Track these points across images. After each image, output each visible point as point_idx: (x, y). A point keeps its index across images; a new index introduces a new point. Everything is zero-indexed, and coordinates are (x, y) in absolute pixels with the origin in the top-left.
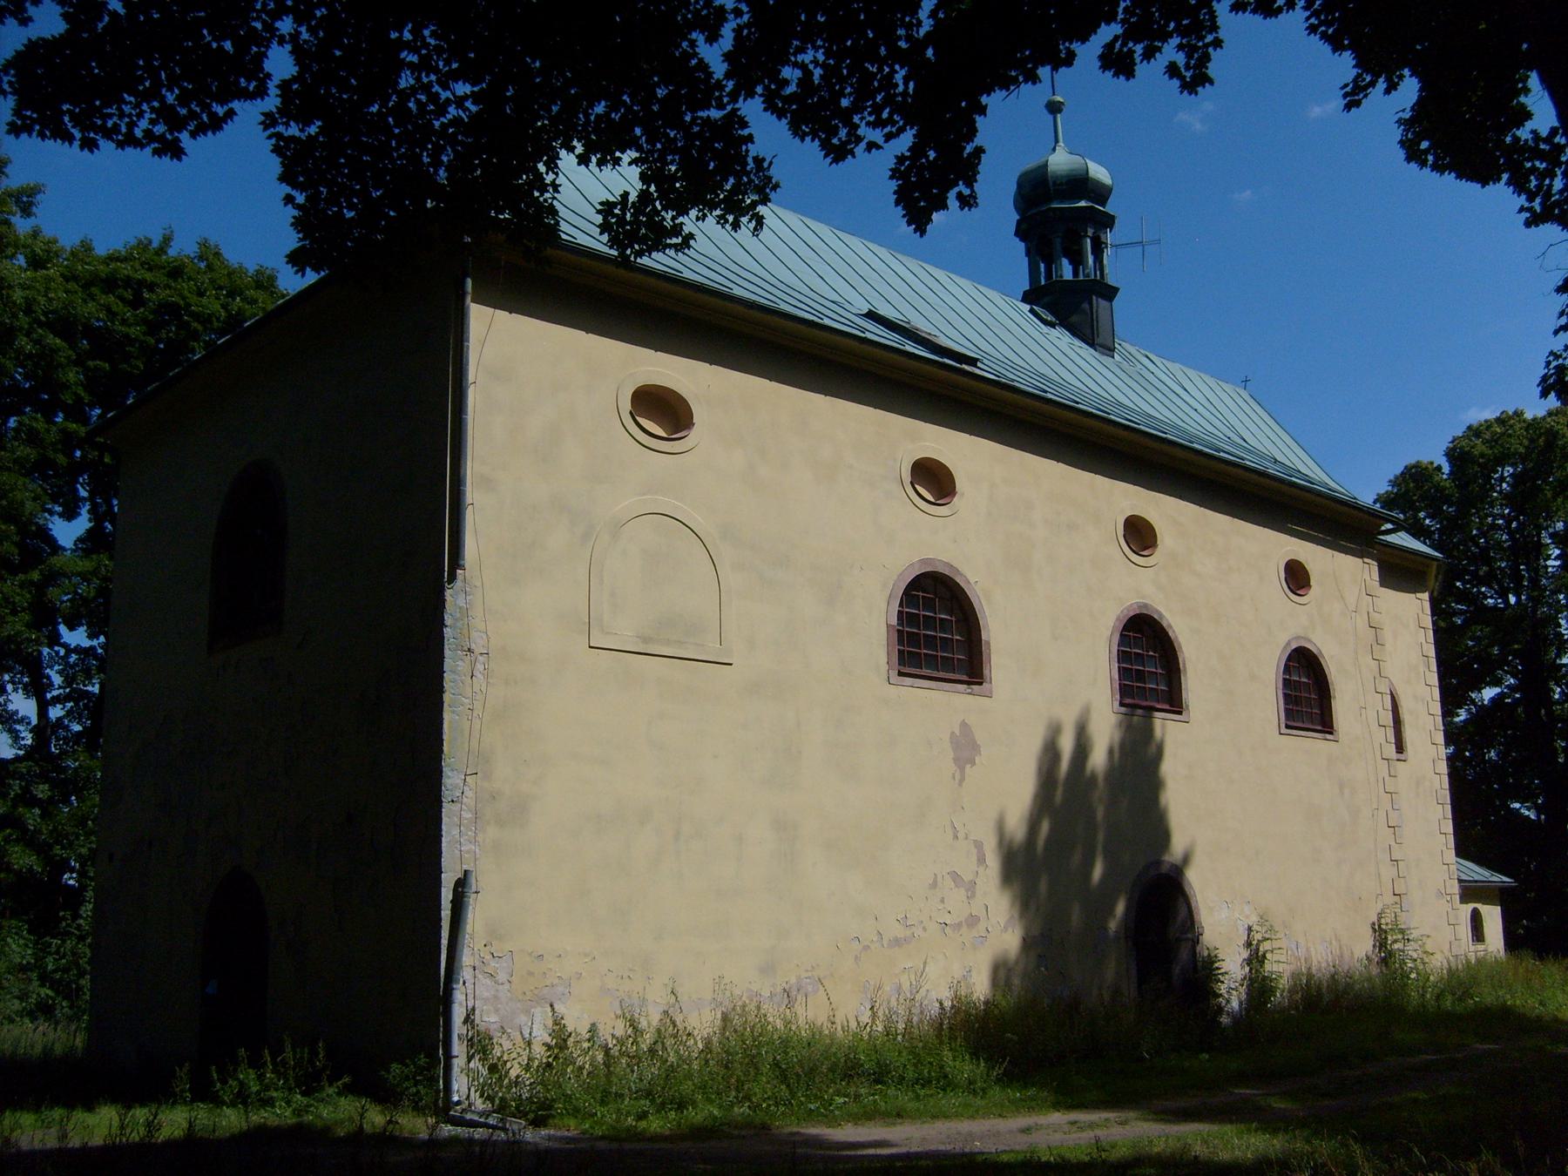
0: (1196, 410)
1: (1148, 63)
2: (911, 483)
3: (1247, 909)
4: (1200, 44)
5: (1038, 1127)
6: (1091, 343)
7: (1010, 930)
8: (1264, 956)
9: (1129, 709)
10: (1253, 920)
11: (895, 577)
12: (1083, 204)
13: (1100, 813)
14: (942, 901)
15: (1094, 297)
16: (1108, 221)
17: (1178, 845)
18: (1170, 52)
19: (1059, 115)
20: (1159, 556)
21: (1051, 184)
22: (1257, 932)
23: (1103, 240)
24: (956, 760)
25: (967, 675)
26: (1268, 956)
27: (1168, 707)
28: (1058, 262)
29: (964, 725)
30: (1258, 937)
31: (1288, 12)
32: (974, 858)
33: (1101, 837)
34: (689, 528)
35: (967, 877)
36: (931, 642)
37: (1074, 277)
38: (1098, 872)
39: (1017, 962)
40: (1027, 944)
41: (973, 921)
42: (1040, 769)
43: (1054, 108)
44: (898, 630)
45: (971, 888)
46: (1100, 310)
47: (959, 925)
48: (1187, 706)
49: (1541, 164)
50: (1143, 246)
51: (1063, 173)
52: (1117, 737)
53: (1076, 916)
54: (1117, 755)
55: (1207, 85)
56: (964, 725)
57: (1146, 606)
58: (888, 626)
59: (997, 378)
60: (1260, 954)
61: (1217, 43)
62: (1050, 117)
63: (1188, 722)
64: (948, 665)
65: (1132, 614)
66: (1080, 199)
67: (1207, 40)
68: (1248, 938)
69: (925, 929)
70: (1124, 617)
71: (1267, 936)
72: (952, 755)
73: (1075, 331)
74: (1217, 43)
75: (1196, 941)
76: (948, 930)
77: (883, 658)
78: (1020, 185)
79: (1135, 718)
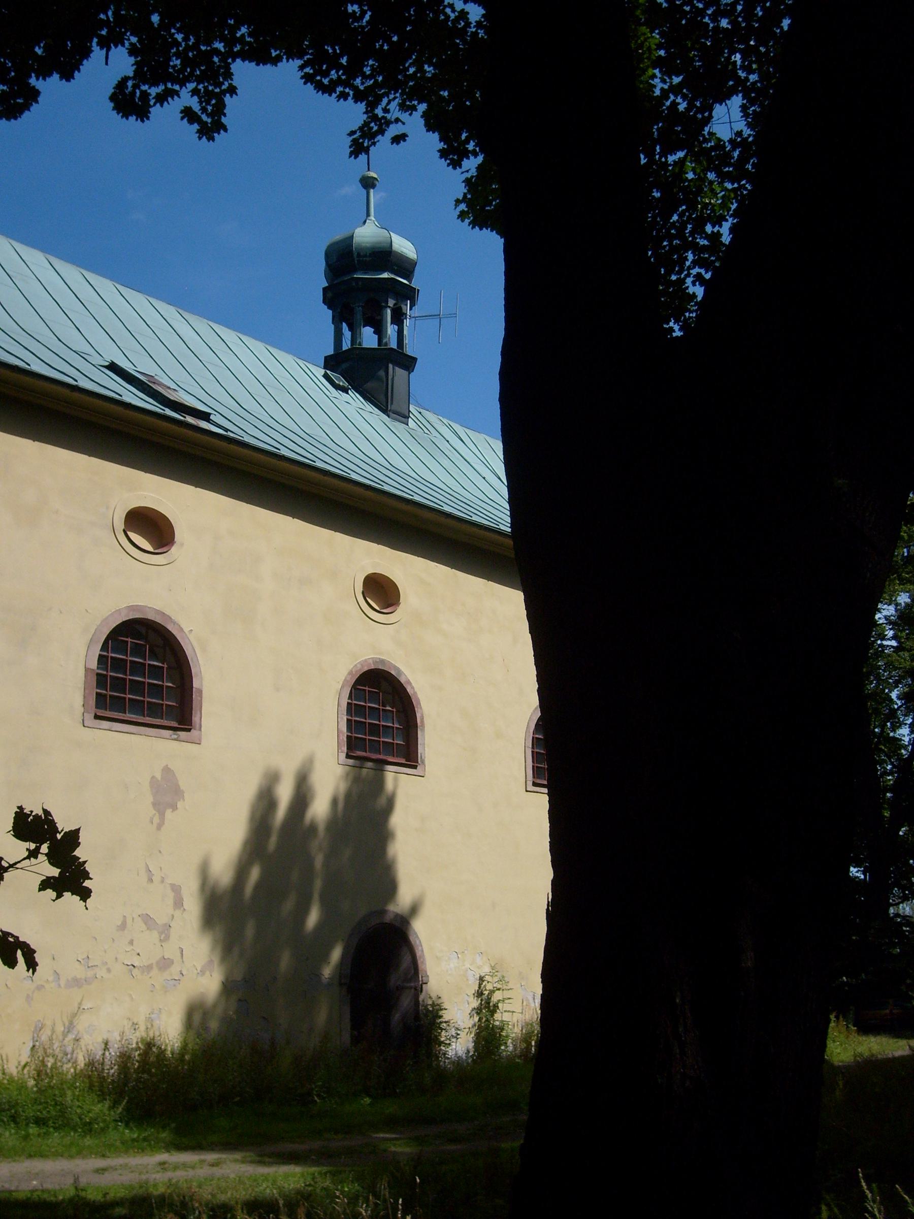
0: (484, 478)
1: (162, 106)
2: (124, 531)
3: (479, 961)
4: (217, 90)
5: (114, 1169)
6: (384, 409)
7: (208, 973)
8: (496, 1006)
9: (357, 761)
10: (486, 969)
11: (98, 623)
12: (385, 275)
13: (319, 861)
14: (131, 942)
15: (391, 366)
16: (410, 294)
17: (405, 896)
18: (186, 98)
19: (372, 191)
20: (400, 613)
21: (355, 255)
22: (488, 982)
23: (404, 311)
24: (155, 804)
25: (177, 722)
26: (500, 1005)
27: (403, 761)
28: (358, 331)
29: (167, 770)
30: (489, 987)
31: (288, 61)
32: (170, 901)
33: (318, 884)
34: (362, 610)
35: (161, 920)
36: (137, 687)
37: (378, 346)
38: (313, 918)
39: (215, 1006)
40: (228, 988)
41: (165, 964)
42: (252, 818)
43: (368, 183)
44: (98, 674)
45: (165, 932)
46: (395, 378)
47: (149, 968)
48: (423, 762)
49: (676, 243)
50: (440, 318)
51: (368, 245)
52: (343, 787)
53: (285, 961)
54: (341, 805)
55: (222, 132)
56: (167, 770)
57: (382, 661)
58: (87, 670)
59: (225, 433)
60: (491, 1004)
61: (232, 90)
62: (364, 191)
63: (423, 777)
64: (155, 710)
65: (366, 669)
66: (384, 271)
67: (224, 87)
68: (480, 987)
69: (109, 970)
70: (356, 672)
71: (499, 986)
72: (150, 799)
73: (369, 397)
74: (232, 90)
75: (419, 990)
76: (135, 972)
77: (78, 700)
78: (328, 255)
79: (364, 771)
